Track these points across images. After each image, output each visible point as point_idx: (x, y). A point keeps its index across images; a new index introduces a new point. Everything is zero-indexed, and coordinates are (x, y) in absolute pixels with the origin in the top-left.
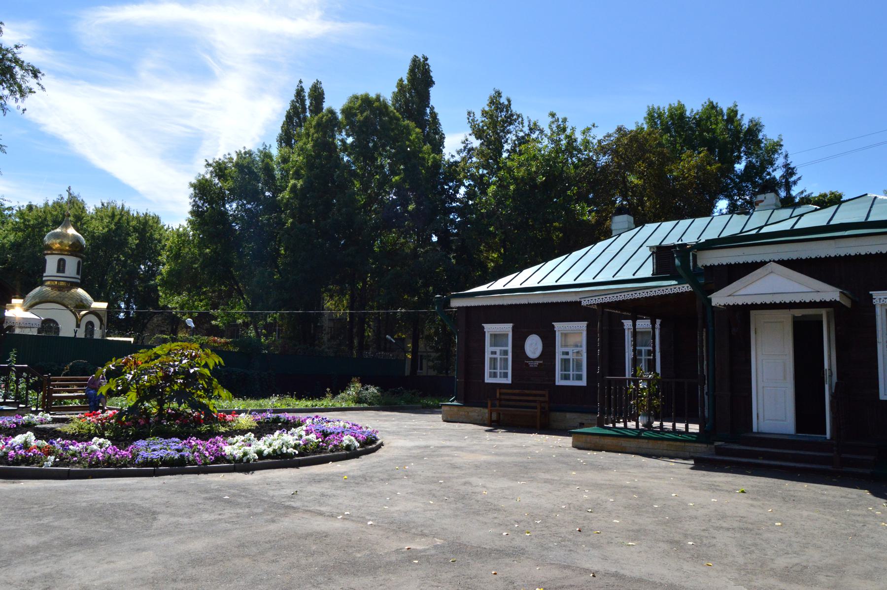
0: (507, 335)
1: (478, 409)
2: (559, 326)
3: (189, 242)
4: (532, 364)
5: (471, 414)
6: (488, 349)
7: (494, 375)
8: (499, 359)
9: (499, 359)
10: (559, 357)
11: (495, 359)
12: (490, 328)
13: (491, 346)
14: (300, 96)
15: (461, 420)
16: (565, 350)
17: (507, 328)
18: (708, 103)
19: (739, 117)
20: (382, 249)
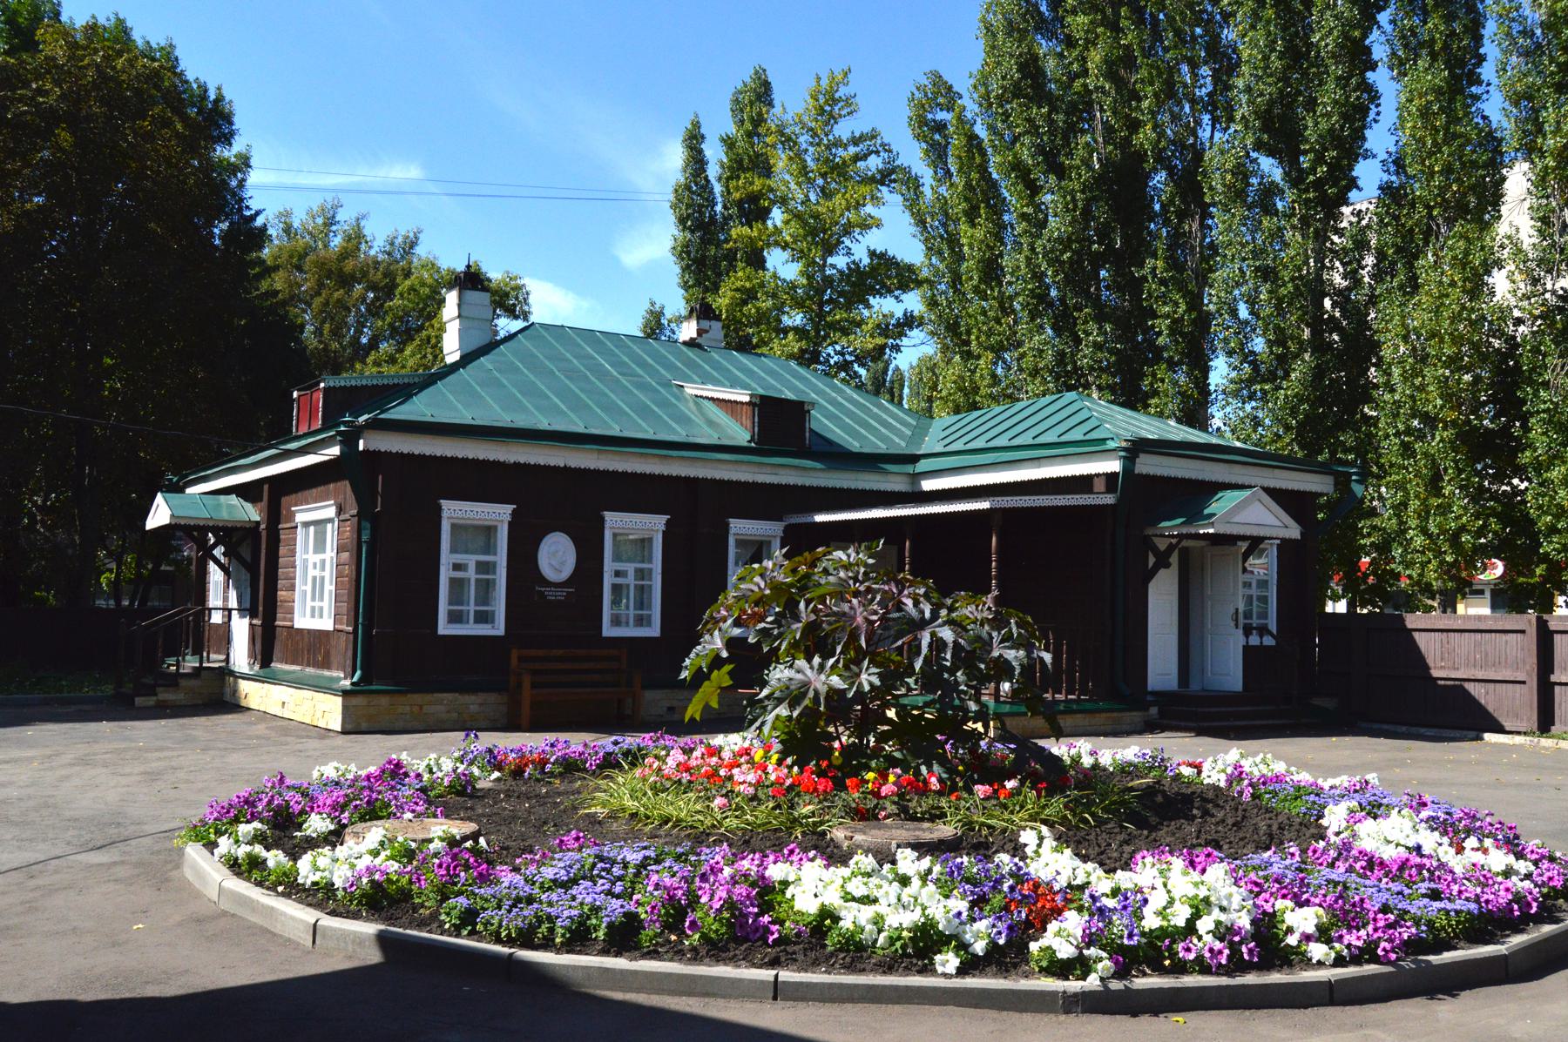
0: (650, 540)
1: (447, 697)
2: (614, 520)
3: (57, 66)
4: (553, 595)
5: (426, 709)
6: (446, 558)
7: (455, 618)
8: (632, 588)
9: (632, 588)
10: (608, 580)
11: (1250, 597)
12: (454, 511)
13: (453, 550)
14: (1266, 197)
15: (400, 725)
16: (620, 566)
17: (500, 514)
18: (113, 20)
19: (212, 96)
20: (24, 222)
